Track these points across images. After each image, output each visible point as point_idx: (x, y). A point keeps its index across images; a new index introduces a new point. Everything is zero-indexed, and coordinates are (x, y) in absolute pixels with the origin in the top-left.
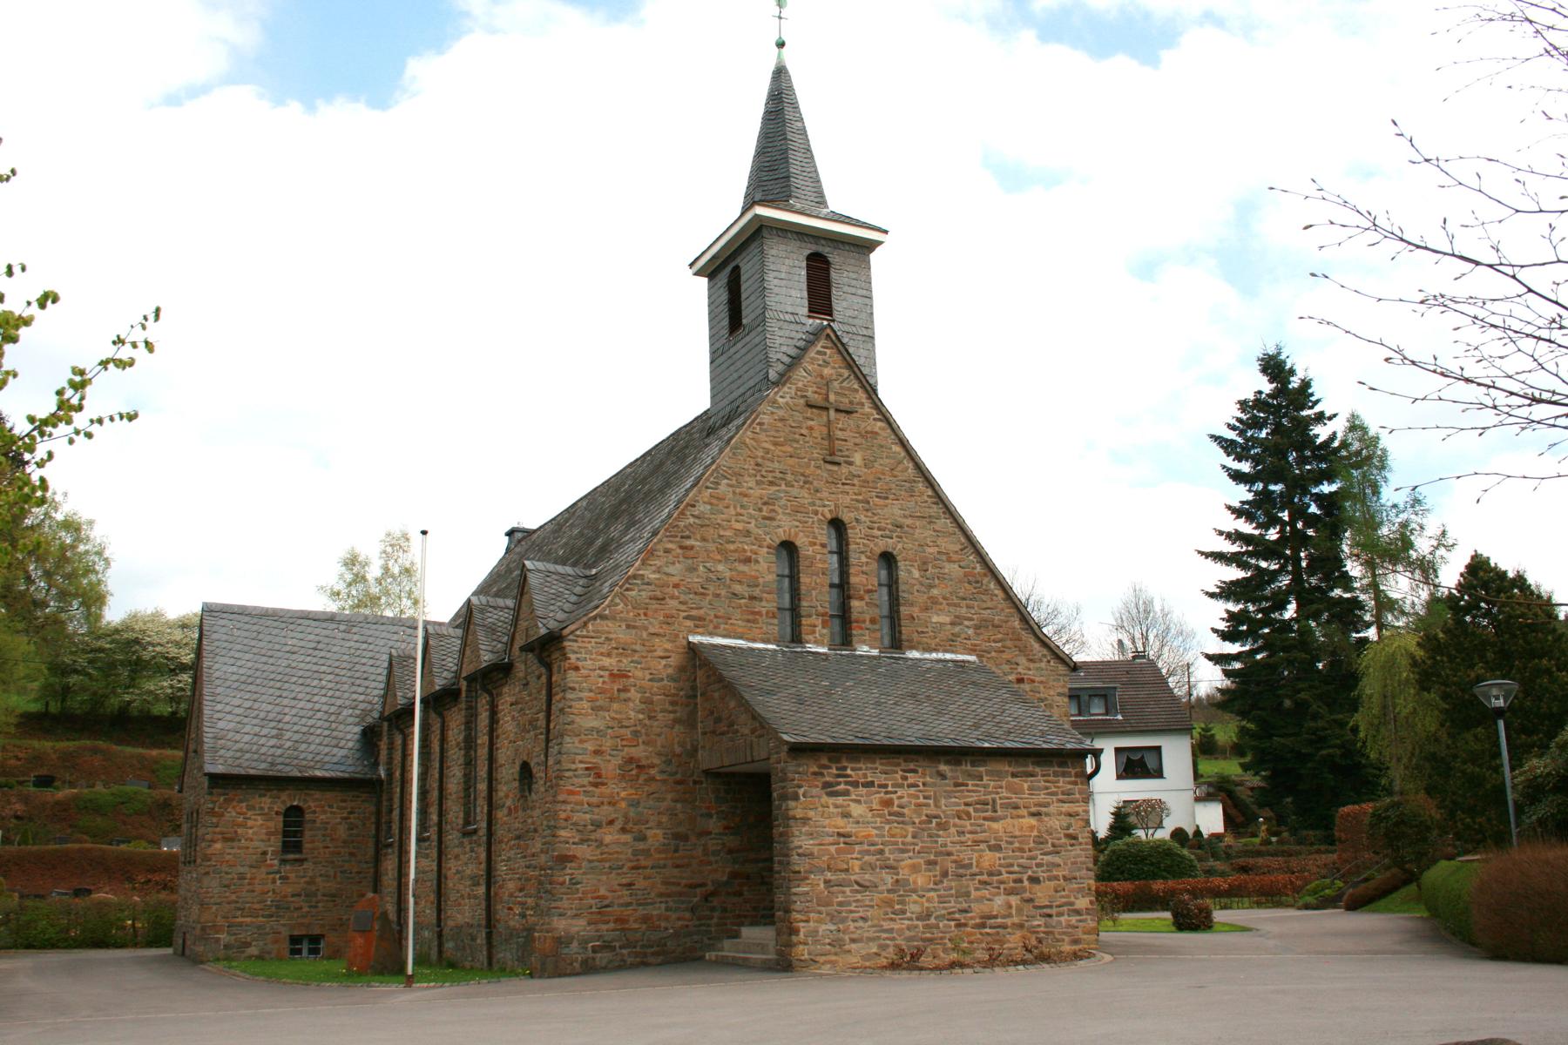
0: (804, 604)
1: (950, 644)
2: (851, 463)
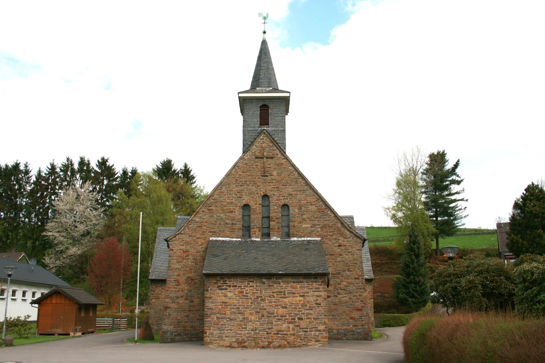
0: (252, 224)
1: (310, 235)
2: (272, 175)
